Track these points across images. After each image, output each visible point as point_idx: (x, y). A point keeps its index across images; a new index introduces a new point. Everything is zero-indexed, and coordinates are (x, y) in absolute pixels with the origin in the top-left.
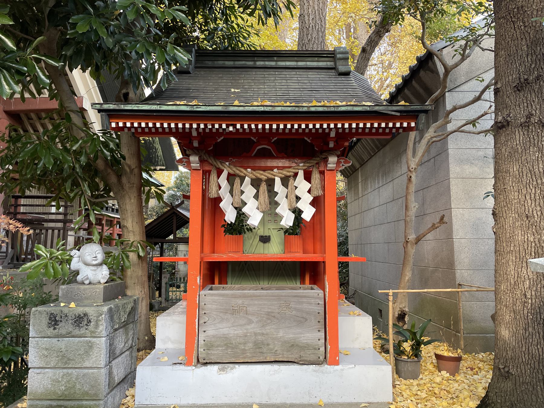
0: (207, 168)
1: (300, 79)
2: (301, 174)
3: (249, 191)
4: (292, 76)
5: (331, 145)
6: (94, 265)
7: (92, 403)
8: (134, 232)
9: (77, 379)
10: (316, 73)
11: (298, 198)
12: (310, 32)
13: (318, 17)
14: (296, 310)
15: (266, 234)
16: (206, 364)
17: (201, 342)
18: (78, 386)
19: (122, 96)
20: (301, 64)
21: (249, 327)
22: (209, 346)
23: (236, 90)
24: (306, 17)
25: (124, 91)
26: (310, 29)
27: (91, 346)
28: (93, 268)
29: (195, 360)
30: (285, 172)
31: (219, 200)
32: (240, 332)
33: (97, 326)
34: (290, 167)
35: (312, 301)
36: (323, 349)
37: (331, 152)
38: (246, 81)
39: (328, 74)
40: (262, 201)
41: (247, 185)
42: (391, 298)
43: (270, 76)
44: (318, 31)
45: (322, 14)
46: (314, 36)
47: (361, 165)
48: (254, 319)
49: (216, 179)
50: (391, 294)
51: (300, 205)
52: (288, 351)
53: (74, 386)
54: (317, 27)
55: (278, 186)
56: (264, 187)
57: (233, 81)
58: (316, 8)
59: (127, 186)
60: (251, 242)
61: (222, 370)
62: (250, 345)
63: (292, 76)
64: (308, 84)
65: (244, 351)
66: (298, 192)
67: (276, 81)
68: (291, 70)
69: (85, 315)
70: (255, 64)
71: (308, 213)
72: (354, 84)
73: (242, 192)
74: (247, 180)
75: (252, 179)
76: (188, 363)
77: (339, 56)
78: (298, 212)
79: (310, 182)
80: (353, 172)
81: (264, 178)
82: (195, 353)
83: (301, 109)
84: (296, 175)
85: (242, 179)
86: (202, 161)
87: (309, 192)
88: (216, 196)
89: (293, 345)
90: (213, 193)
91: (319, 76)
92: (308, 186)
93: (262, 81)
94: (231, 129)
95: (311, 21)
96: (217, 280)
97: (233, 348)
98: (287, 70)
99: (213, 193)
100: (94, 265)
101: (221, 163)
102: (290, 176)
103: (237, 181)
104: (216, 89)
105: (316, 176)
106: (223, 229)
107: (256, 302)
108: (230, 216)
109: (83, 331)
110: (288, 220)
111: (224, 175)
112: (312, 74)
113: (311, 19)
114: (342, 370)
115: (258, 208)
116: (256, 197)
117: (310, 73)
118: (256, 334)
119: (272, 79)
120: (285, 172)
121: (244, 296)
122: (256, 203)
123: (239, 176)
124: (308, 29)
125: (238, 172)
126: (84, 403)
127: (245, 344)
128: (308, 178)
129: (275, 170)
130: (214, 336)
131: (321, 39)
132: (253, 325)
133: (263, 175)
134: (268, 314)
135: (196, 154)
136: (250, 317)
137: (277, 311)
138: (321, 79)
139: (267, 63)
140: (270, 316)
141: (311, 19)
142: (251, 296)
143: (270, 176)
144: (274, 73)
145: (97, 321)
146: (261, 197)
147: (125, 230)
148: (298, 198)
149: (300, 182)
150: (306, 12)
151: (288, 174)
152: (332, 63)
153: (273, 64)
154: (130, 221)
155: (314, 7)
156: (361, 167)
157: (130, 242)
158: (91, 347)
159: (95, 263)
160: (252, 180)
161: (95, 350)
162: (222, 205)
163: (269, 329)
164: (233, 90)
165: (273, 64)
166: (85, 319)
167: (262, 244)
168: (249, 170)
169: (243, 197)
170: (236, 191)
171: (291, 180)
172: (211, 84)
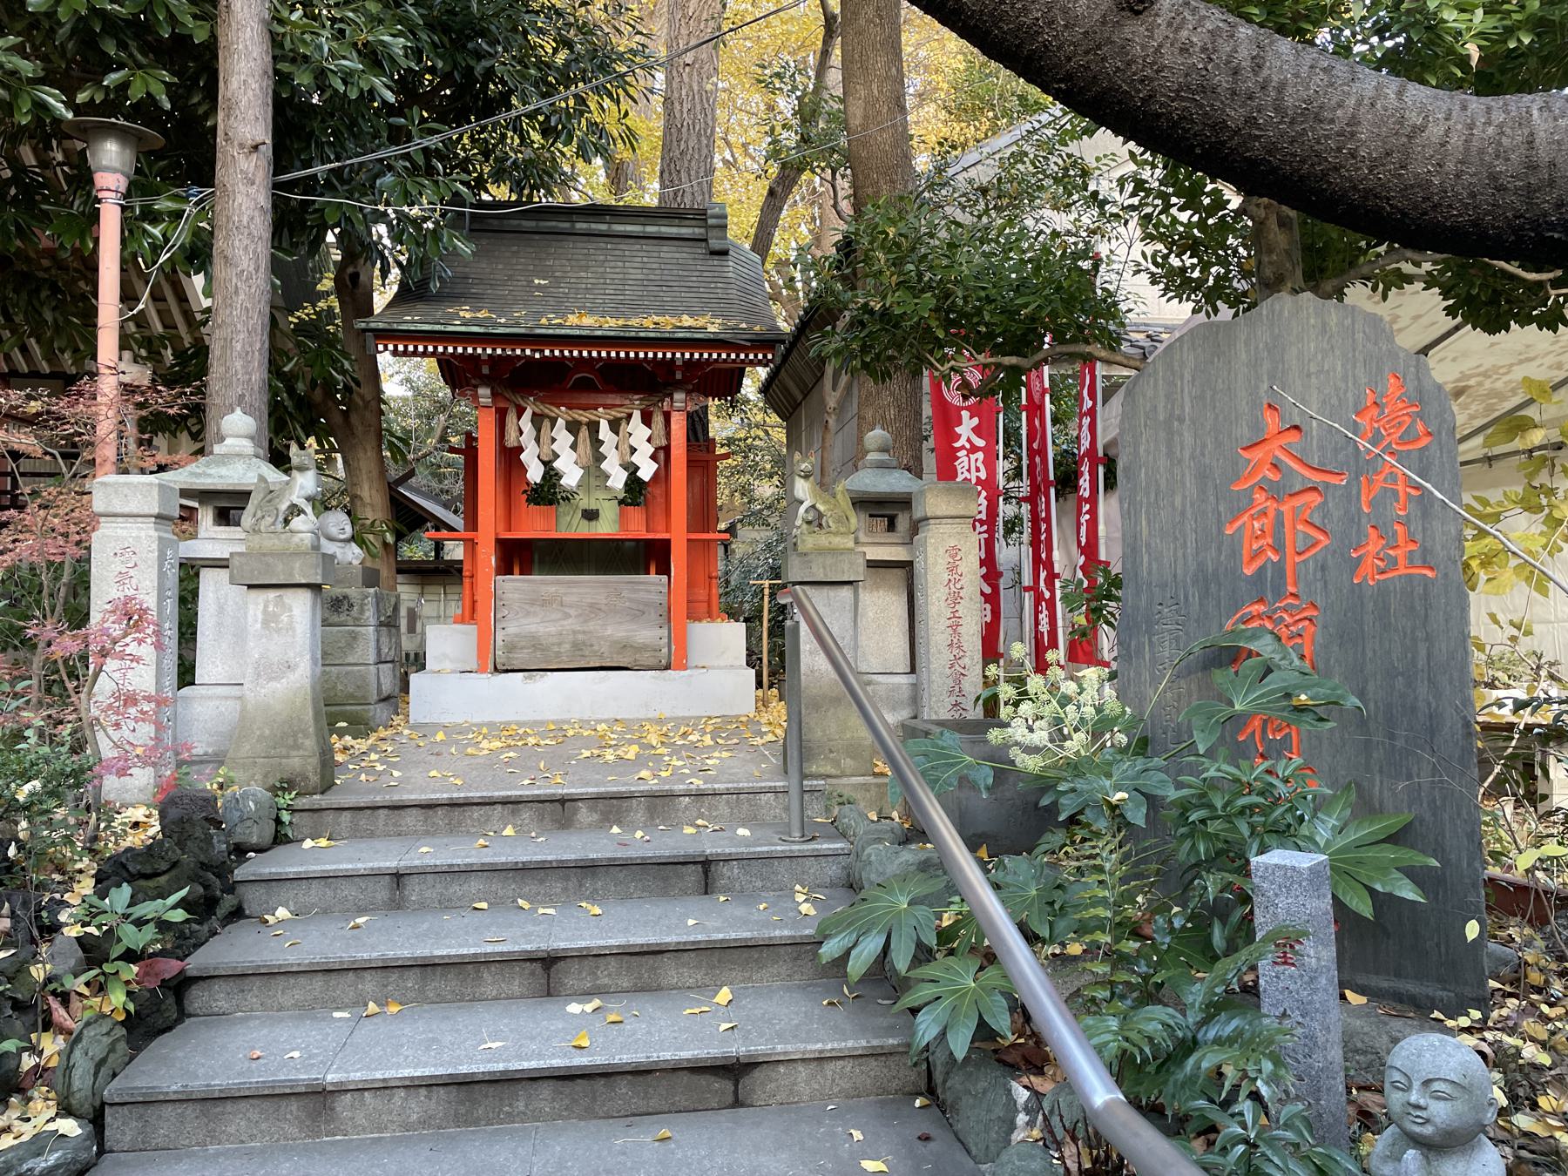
0: (502, 405)
1: (645, 260)
2: (637, 415)
3: (563, 438)
4: (634, 253)
5: (679, 376)
6: (341, 541)
7: (359, 708)
8: (372, 505)
9: (338, 678)
10: (674, 249)
11: (633, 450)
12: (685, 136)
13: (698, 107)
14: (630, 600)
15: (593, 507)
16: (507, 671)
17: (499, 643)
18: (340, 687)
19: (347, 278)
20: (651, 229)
21: (565, 623)
22: (511, 648)
23: (542, 282)
24: (677, 104)
25: (350, 270)
26: (684, 130)
27: (354, 637)
28: (339, 544)
29: (491, 666)
30: (615, 413)
31: (520, 449)
32: (552, 629)
33: (362, 611)
34: (621, 406)
35: (652, 588)
36: (665, 650)
37: (678, 386)
38: (557, 262)
39: (693, 250)
40: (582, 453)
41: (560, 430)
42: (767, 592)
43: (599, 252)
44: (699, 135)
45: (708, 101)
46: (691, 144)
47: (805, 396)
48: (572, 612)
49: (515, 420)
50: (767, 585)
51: (635, 459)
52: (619, 653)
53: (334, 687)
54: (697, 128)
55: (605, 432)
56: (584, 433)
57: (537, 262)
58: (696, 88)
59: (359, 429)
60: (569, 518)
61: (530, 678)
62: (567, 646)
63: (634, 253)
64: (657, 272)
65: (558, 654)
66: (632, 441)
67: (606, 264)
68: (633, 241)
69: (346, 597)
70: (573, 227)
71: (647, 471)
72: (730, 275)
73: (554, 440)
74: (561, 422)
75: (567, 422)
76: (481, 670)
77: (711, 221)
78: (632, 469)
79: (649, 426)
80: (795, 409)
81: (585, 420)
82: (491, 656)
83: (627, 335)
84: (630, 416)
85: (553, 422)
86: (494, 395)
87: (649, 440)
88: (516, 444)
89: (625, 647)
90: (511, 441)
91: (677, 255)
92: (648, 432)
93: (583, 263)
94: (537, 356)
95: (685, 115)
96: (517, 569)
97: (543, 650)
98: (628, 241)
99: (511, 441)
100: (341, 541)
101: (522, 398)
102: (621, 419)
103: (546, 423)
104: (510, 278)
105: (658, 419)
106: (525, 496)
107: (575, 590)
108: (535, 474)
109: (343, 618)
110: (618, 480)
111: (528, 415)
112: (668, 252)
113: (685, 110)
114: (691, 676)
115: (576, 463)
116: (574, 447)
117: (665, 249)
118: (574, 632)
119: (602, 258)
120: (615, 413)
121: (558, 583)
122: (574, 455)
123: (548, 417)
124: (679, 130)
125: (547, 411)
126: (348, 708)
127: (559, 644)
128: (647, 420)
129: (600, 410)
130: (516, 635)
131: (705, 151)
132: (570, 621)
133: (583, 416)
134: (592, 605)
135: (486, 385)
136: (567, 610)
137: (605, 601)
138: (680, 261)
139: (593, 226)
140: (594, 609)
141: (685, 110)
142: (568, 582)
143: (593, 418)
144: (603, 245)
145: (362, 606)
146: (581, 447)
147: (358, 503)
148: (633, 450)
149: (637, 426)
150: (676, 95)
151: (619, 415)
152: (702, 231)
153: (604, 227)
154: (366, 487)
155: (691, 87)
156: (804, 398)
157: (368, 522)
158: (355, 638)
159: (342, 537)
160: (568, 423)
161: (361, 642)
162: (522, 457)
163: (591, 626)
164: (537, 281)
165: (604, 227)
166: (345, 602)
167: (585, 522)
168: (563, 408)
169: (554, 447)
170: (545, 437)
171: (623, 423)
172: (500, 267)
